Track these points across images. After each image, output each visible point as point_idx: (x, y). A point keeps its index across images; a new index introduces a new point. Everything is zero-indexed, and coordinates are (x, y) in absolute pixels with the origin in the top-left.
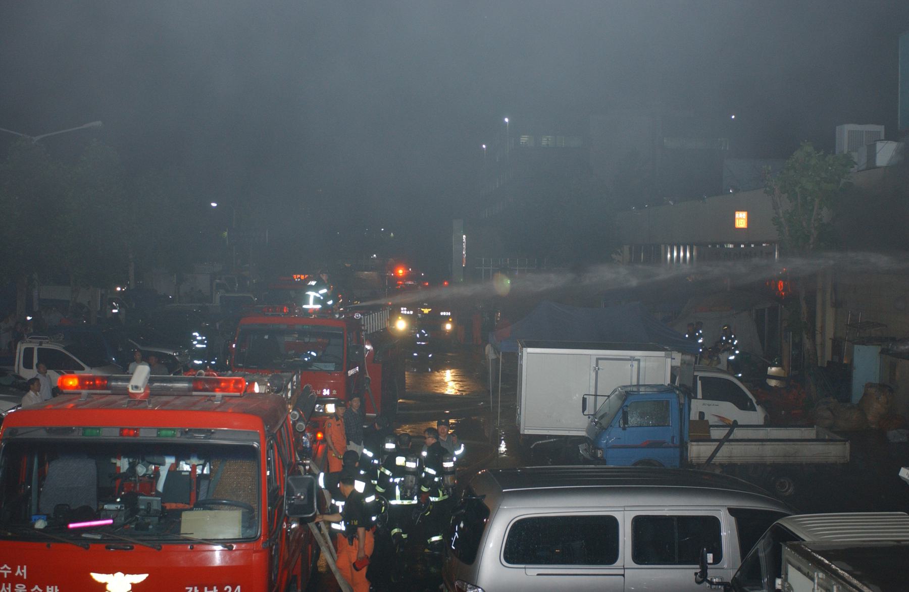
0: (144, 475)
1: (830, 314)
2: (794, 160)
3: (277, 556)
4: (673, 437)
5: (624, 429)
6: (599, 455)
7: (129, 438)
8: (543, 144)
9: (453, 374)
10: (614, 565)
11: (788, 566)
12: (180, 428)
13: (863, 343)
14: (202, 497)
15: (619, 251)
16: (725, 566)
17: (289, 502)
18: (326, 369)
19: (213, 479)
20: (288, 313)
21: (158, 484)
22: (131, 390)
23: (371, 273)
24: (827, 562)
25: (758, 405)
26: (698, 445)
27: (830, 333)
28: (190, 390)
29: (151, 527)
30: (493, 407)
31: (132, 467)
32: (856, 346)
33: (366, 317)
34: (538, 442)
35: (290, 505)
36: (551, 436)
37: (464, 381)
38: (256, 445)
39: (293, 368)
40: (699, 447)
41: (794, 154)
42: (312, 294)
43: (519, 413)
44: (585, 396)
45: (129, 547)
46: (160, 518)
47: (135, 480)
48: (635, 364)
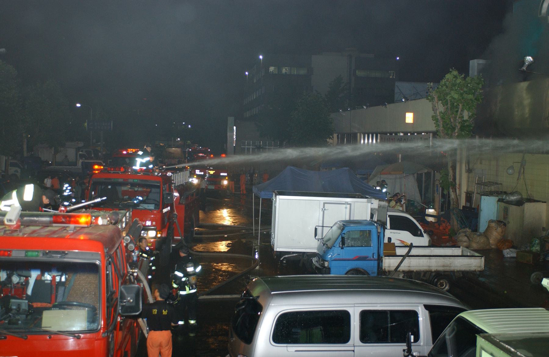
0: (18, 283)
1: (465, 175)
2: (446, 80)
3: (113, 342)
4: (373, 254)
5: (342, 248)
6: (326, 265)
7: (3, 257)
8: (283, 72)
9: (229, 212)
10: (346, 344)
11: (482, 351)
12: (42, 250)
13: (487, 195)
14: (60, 299)
15: (331, 137)
16: (422, 344)
17: (122, 304)
18: (149, 208)
19: (68, 286)
20: (124, 171)
21: (28, 290)
22: (6, 222)
23: (177, 149)
24: (513, 350)
25: (425, 233)
26: (389, 259)
27: (464, 189)
28: (51, 223)
29: (20, 322)
30: (255, 233)
31: (9, 277)
32: (482, 197)
33: (175, 175)
34: (285, 256)
35: (123, 306)
36: (294, 253)
37: (236, 217)
38: (98, 262)
39: (126, 207)
40: (390, 260)
41: (446, 76)
42: (139, 161)
43: (273, 237)
44: (316, 227)
45: (3, 337)
46: (27, 316)
47: (11, 287)
48: (348, 206)
